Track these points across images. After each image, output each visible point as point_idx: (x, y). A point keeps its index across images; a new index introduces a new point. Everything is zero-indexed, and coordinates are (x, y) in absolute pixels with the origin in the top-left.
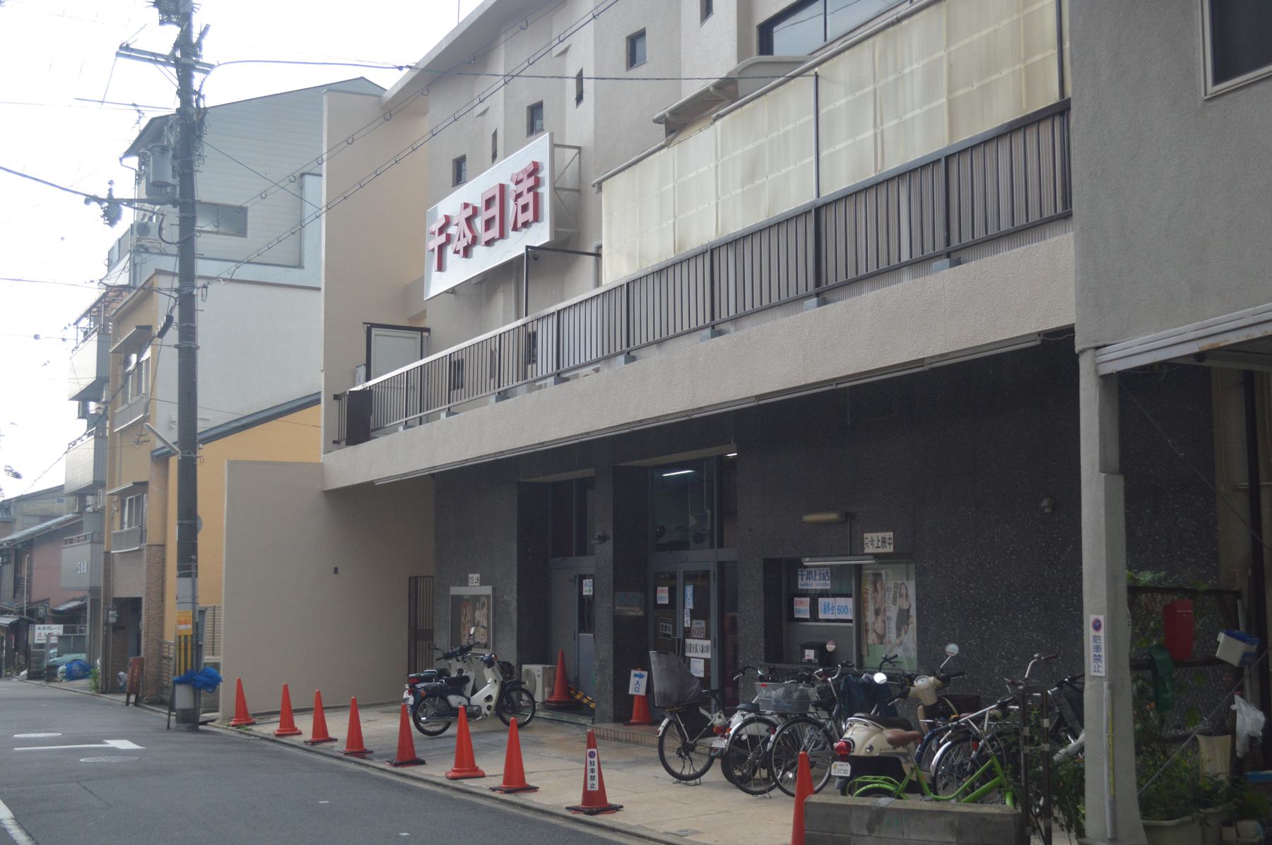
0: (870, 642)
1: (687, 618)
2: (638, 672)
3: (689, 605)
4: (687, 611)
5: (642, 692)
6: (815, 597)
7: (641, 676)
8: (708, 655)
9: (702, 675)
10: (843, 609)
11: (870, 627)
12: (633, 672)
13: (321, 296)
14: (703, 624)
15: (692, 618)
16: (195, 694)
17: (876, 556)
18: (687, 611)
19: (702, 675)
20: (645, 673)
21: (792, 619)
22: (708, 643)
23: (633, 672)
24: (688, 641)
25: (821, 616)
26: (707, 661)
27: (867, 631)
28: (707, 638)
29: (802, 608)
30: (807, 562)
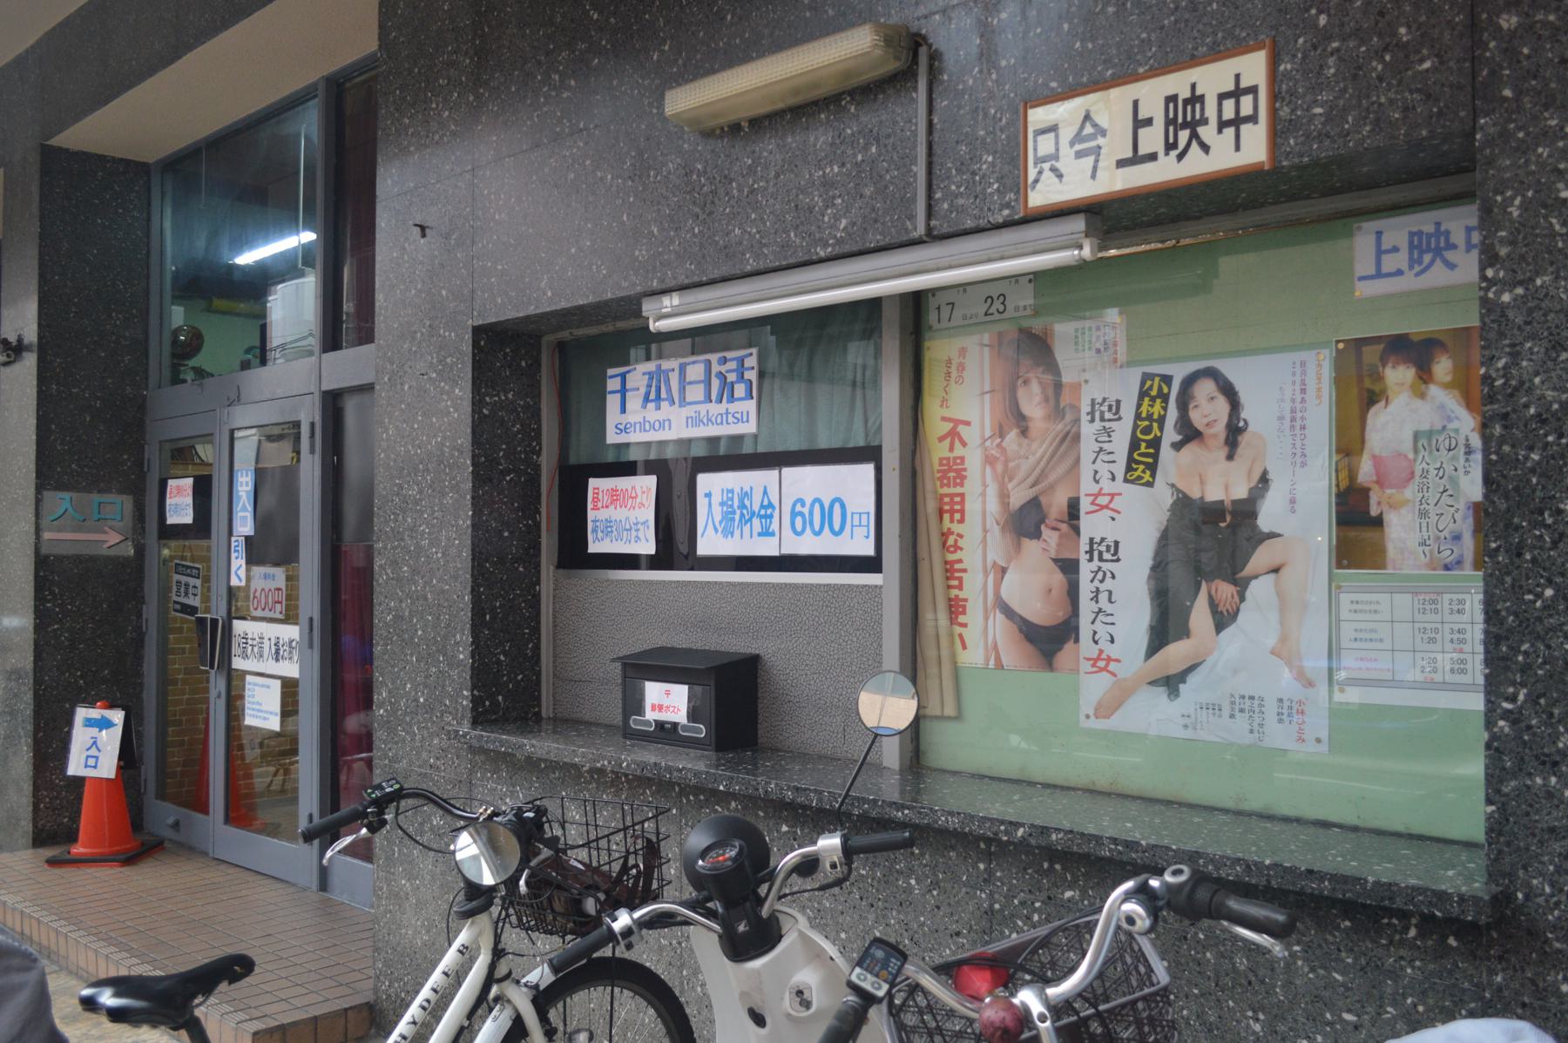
0: (973, 656)
1: (238, 562)
2: (95, 713)
3: (245, 525)
4: (238, 544)
5: (107, 767)
6: (675, 477)
7: (105, 724)
8: (291, 670)
9: (274, 724)
10: (831, 514)
11: (973, 587)
12: (82, 713)
13: (30, 361)
14: (279, 575)
15: (250, 561)
16: (1024, 621)
17: (1105, 216)
18: (238, 544)
19: (274, 724)
20: (118, 716)
21: (575, 554)
22: (291, 632)
23: (82, 713)
24: (239, 626)
25: (709, 543)
26: (290, 688)
27: (956, 608)
28: (289, 618)
29: (622, 516)
30: (669, 314)
